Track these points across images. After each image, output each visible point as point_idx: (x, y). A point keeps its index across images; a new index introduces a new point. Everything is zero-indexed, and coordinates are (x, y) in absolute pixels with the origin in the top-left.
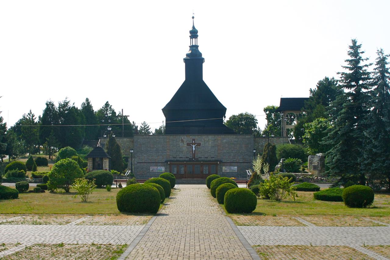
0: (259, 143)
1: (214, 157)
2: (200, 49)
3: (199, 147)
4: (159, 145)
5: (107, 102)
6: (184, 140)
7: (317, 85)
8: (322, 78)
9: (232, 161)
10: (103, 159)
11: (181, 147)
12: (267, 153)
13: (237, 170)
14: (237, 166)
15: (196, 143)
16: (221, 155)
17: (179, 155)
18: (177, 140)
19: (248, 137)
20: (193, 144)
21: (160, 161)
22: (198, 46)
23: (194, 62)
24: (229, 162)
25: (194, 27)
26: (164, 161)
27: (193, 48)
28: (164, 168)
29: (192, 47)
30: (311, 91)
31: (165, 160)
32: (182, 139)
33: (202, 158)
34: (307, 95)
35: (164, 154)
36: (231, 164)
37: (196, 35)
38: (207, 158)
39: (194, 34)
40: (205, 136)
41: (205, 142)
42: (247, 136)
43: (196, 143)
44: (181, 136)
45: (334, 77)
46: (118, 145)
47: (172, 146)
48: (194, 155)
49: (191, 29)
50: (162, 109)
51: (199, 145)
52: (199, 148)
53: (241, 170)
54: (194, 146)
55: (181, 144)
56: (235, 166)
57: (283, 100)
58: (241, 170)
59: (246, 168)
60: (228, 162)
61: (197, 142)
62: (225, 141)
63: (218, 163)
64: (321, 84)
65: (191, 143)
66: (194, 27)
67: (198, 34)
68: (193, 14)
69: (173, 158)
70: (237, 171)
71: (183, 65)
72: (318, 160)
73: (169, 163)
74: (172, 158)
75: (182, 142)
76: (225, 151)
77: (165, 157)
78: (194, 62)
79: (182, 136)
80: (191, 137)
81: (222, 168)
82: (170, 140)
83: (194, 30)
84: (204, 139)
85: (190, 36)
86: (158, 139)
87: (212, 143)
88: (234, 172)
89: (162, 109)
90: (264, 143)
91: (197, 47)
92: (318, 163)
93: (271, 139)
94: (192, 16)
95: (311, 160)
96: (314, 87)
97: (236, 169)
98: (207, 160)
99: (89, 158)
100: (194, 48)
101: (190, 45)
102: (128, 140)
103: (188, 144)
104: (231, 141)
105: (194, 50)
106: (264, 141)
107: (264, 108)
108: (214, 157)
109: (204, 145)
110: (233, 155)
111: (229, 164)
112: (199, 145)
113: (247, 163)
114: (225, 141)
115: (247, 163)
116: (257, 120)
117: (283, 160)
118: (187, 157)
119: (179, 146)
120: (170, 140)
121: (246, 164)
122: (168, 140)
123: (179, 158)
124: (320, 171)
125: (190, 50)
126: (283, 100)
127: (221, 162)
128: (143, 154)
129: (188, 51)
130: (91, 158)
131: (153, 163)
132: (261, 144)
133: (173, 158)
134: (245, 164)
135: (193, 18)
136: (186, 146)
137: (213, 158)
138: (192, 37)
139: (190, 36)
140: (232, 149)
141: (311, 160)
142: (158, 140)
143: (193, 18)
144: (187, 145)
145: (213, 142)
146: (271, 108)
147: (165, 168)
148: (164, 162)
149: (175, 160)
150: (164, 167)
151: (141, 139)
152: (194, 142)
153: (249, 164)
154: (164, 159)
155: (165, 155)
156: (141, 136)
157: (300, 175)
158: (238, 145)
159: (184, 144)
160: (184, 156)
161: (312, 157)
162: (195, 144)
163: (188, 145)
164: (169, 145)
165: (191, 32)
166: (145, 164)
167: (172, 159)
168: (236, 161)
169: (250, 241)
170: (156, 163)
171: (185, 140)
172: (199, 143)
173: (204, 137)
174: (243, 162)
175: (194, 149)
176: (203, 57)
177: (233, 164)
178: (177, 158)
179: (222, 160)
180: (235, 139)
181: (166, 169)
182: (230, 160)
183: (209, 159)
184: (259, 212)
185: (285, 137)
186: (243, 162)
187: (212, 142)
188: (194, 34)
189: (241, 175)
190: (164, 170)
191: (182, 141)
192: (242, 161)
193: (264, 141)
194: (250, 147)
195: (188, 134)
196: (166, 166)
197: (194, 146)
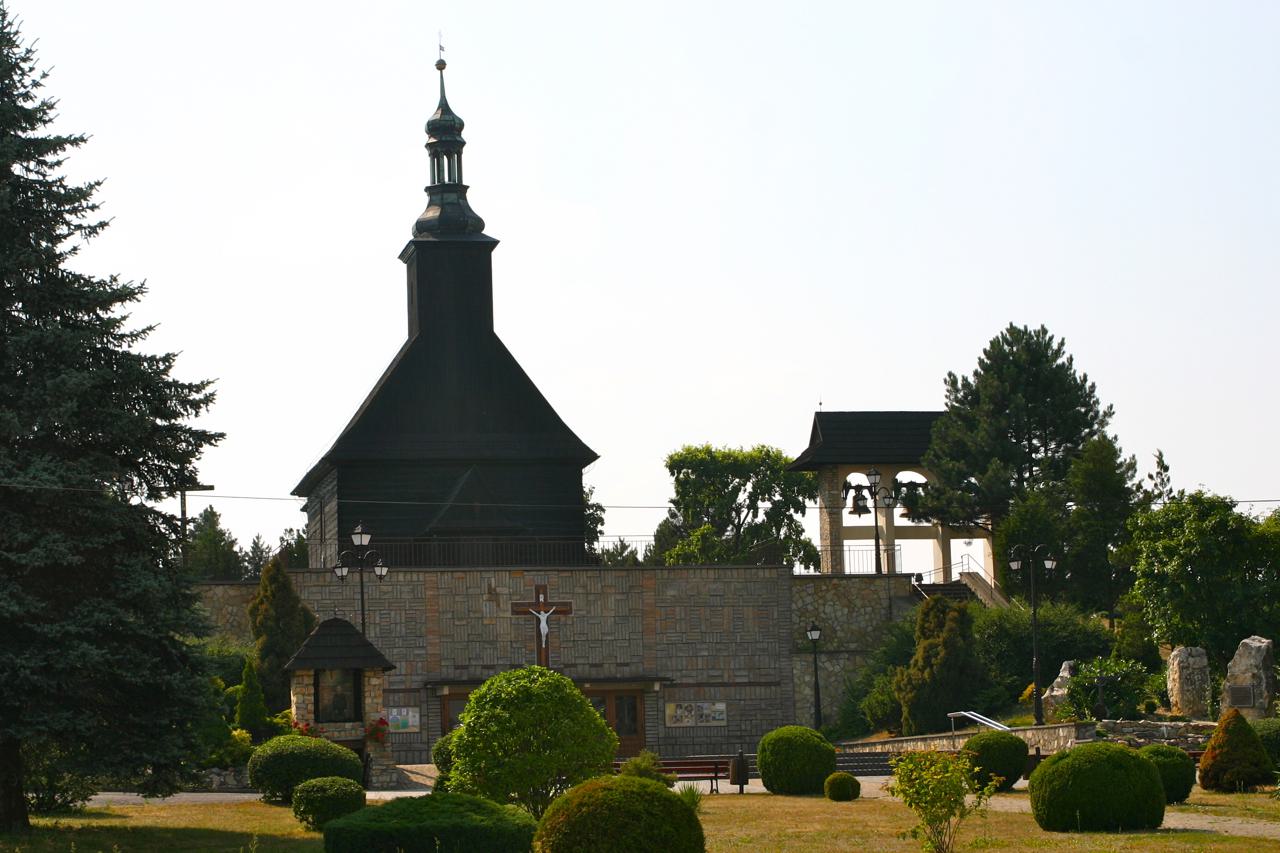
1: (627, 665)
4: (393, 613)
5: (1011, 324)
6: (498, 590)
7: (983, 356)
8: (998, 329)
9: (703, 678)
10: (368, 674)
11: (486, 622)
12: (945, 644)
13: (724, 716)
15: (552, 605)
16: (659, 654)
18: (471, 591)
20: (538, 606)
21: (402, 682)
23: (450, 261)
24: (691, 681)
25: (444, 106)
26: (416, 681)
27: (445, 196)
28: (418, 716)
29: (443, 192)
30: (952, 380)
31: (419, 678)
32: (490, 585)
33: (580, 668)
34: (935, 400)
35: (417, 652)
37: (458, 139)
38: (600, 665)
39: (446, 136)
40: (590, 574)
41: (591, 598)
43: (552, 605)
44: (485, 575)
45: (1046, 327)
46: (305, 611)
47: (450, 616)
48: (543, 653)
49: (431, 112)
50: (819, 415)
51: (564, 610)
52: (566, 624)
53: (742, 715)
54: (543, 617)
55: (487, 608)
56: (720, 701)
57: (825, 423)
58: (742, 715)
59: (763, 706)
60: (688, 685)
61: (556, 600)
62: (671, 592)
63: (657, 687)
64: (995, 352)
65: (530, 605)
66: (444, 106)
67: (462, 136)
68: (441, 48)
69: (457, 667)
70: (728, 721)
71: (396, 280)
72: (1256, 667)
74: (451, 671)
75: (489, 600)
77: (420, 664)
78: (450, 261)
79: (491, 575)
80: (529, 576)
81: (664, 711)
82: (441, 592)
83: (447, 117)
84: (584, 587)
85: (428, 146)
86: (390, 588)
87: (617, 601)
88: (715, 723)
89: (819, 415)
90: (809, 599)
92: (1254, 675)
93: (840, 585)
94: (438, 59)
95: (1187, 668)
96: (967, 368)
97: (722, 713)
98: (602, 676)
99: (298, 673)
100: (452, 197)
101: (429, 184)
102: (232, 592)
103: (519, 610)
104: (699, 594)
105: (448, 204)
106: (811, 591)
107: (671, 458)
108: (627, 665)
109: (584, 613)
110: (706, 654)
111: (692, 690)
112: (564, 610)
113: (768, 684)
114: (671, 592)
115: (768, 684)
116: (603, 510)
117: (1074, 671)
119: (477, 615)
120: (441, 592)
121: (763, 689)
122: (429, 593)
123: (587, 667)
124: (1266, 710)
125: (430, 204)
126: (825, 423)
129: (417, 206)
130: (309, 669)
132: (800, 604)
133: (457, 667)
135: (441, 65)
136: (509, 614)
137: (627, 669)
138: (435, 151)
139: (428, 146)
140: (703, 628)
141: (1187, 668)
142: (385, 593)
143: (441, 65)
144: (514, 612)
145: (624, 597)
146: (700, 456)
147: (421, 716)
148: (415, 686)
149: (465, 678)
150: (417, 709)
151: (314, 589)
152: (542, 599)
153: (773, 688)
154: (418, 675)
155: (419, 655)
156: (314, 577)
157: (1180, 728)
158: (726, 610)
159: (498, 605)
160: (501, 662)
161: (1190, 655)
162: (547, 606)
163: (517, 613)
164: (437, 611)
167: (452, 676)
168: (722, 676)
171: (505, 591)
172: (565, 604)
174: (750, 684)
175: (544, 628)
176: (488, 231)
177: (707, 689)
178: (472, 670)
181: (425, 719)
182: (694, 673)
183: (609, 670)
186: (750, 684)
187: (619, 597)
188: (446, 136)
189: (740, 737)
190: (417, 723)
191: (493, 595)
192: (746, 680)
193: (811, 591)
194: (776, 616)
195: (454, 565)
196: (424, 706)
197: (543, 617)
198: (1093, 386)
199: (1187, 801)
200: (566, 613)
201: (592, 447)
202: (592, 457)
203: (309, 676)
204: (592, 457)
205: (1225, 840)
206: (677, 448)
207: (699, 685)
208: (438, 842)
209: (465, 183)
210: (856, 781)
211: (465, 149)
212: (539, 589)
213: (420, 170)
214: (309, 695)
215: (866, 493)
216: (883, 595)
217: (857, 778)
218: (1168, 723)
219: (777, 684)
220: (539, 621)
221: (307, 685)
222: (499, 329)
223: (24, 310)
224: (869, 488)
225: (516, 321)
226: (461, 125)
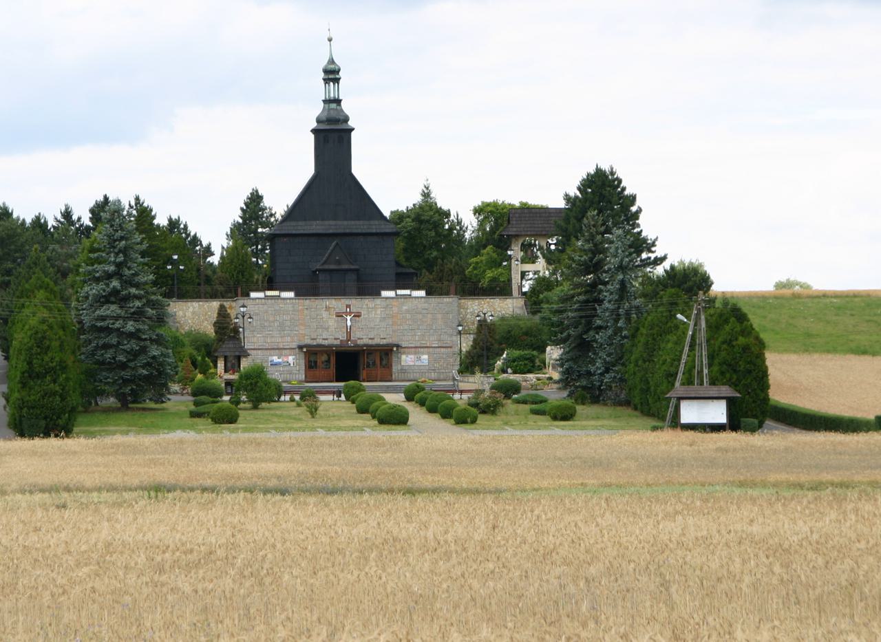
0: (467, 309)
2: (346, 107)
3: (357, 319)
9: (418, 345)
14: (429, 354)
17: (321, 335)
19: (448, 300)
20: (347, 314)
22: (341, 101)
26: (294, 345)
33: (364, 340)
36: (417, 349)
39: (332, 75)
42: (445, 300)
49: (324, 62)
54: (349, 318)
55: (325, 314)
60: (412, 348)
62: (405, 308)
66: (332, 61)
73: (305, 350)
76: (406, 327)
80: (343, 301)
91: (338, 101)
100: (333, 106)
112: (358, 315)
114: (405, 308)
118: (335, 339)
122: (300, 307)
127: (398, 346)
128: (255, 333)
129: (318, 109)
131: (274, 349)
134: (442, 349)
135: (330, 40)
143: (330, 40)
162: (350, 313)
165: (326, 71)
166: (259, 351)
169: (515, 229)
170: (279, 350)
173: (366, 301)
174: (439, 347)
175: (349, 323)
179: (400, 343)
180: (424, 305)
184: (857, 357)
185: (516, 298)
186: (439, 347)
188: (332, 75)
197: (349, 318)
198: (639, 211)
199: (409, 423)
200: (359, 316)
205: (602, 426)
206: (478, 203)
207: (416, 347)
208: (504, 356)
209: (340, 98)
212: (348, 306)
213: (319, 89)
216: (510, 306)
218: (244, 426)
219: (451, 347)
222: (354, 171)
225: (361, 169)
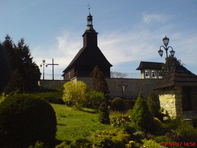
39: (90, 18)
65: (121, 85)
100: (91, 27)
144: (118, 86)
188: (90, 18)
197: (124, 87)
201: (111, 63)
202: (112, 66)
203: (179, 90)
204: (112, 66)
210: (51, 106)
211: (93, 20)
213: (86, 22)
214: (180, 98)
215: (154, 73)
217: (53, 105)
220: (122, 88)
221: (179, 94)
223: (23, 58)
224: (148, 73)
226: (92, 17)
